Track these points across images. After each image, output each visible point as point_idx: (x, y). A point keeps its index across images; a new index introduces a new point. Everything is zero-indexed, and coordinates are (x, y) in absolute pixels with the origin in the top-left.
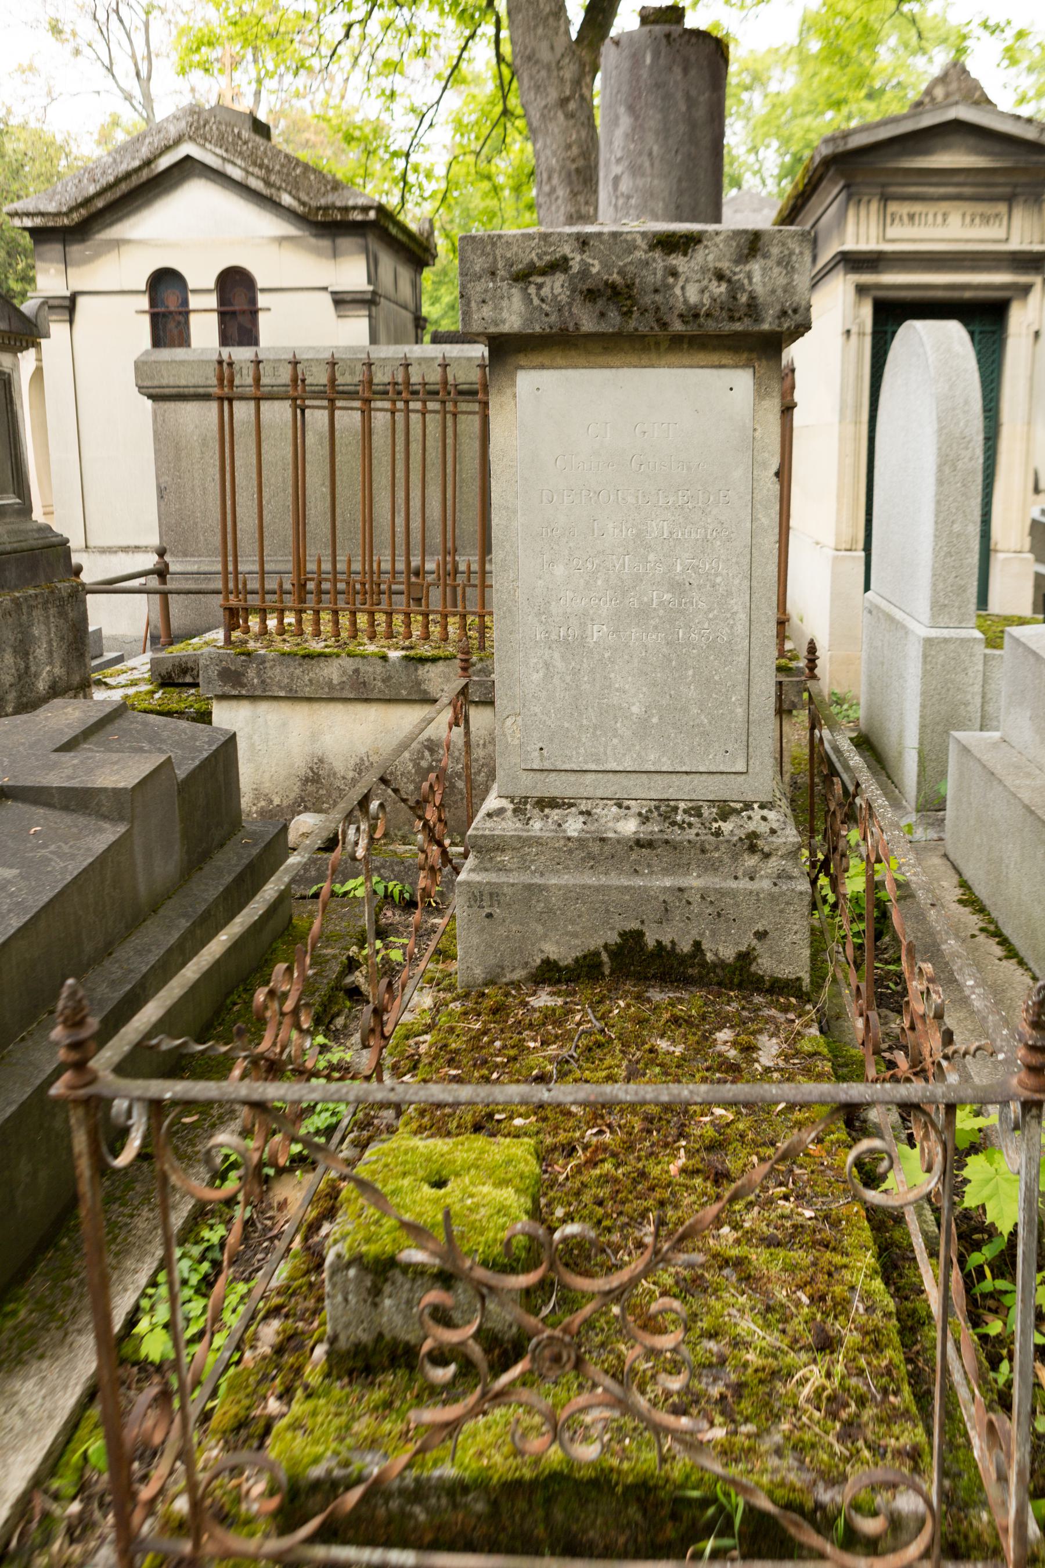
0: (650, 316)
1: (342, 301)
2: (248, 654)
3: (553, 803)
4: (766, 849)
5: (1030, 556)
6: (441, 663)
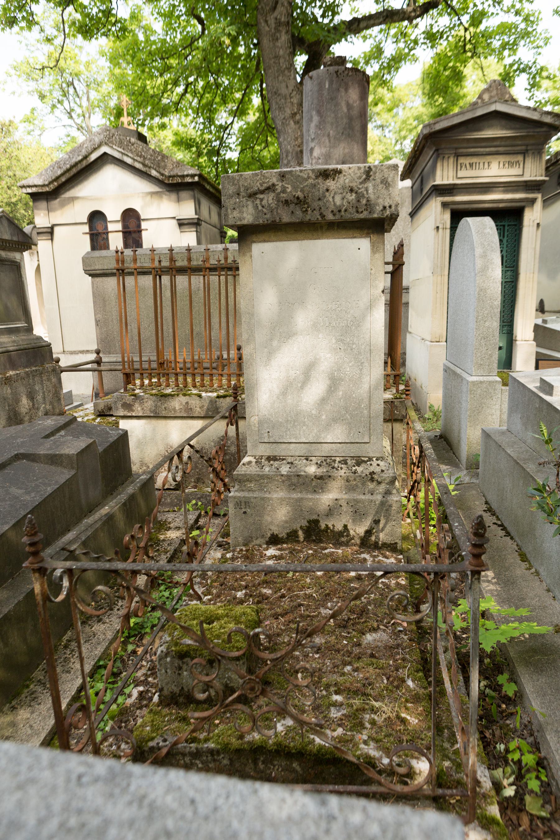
0: (317, 213)
1: (182, 224)
2: (135, 395)
3: (275, 458)
4: (379, 480)
5: (534, 343)
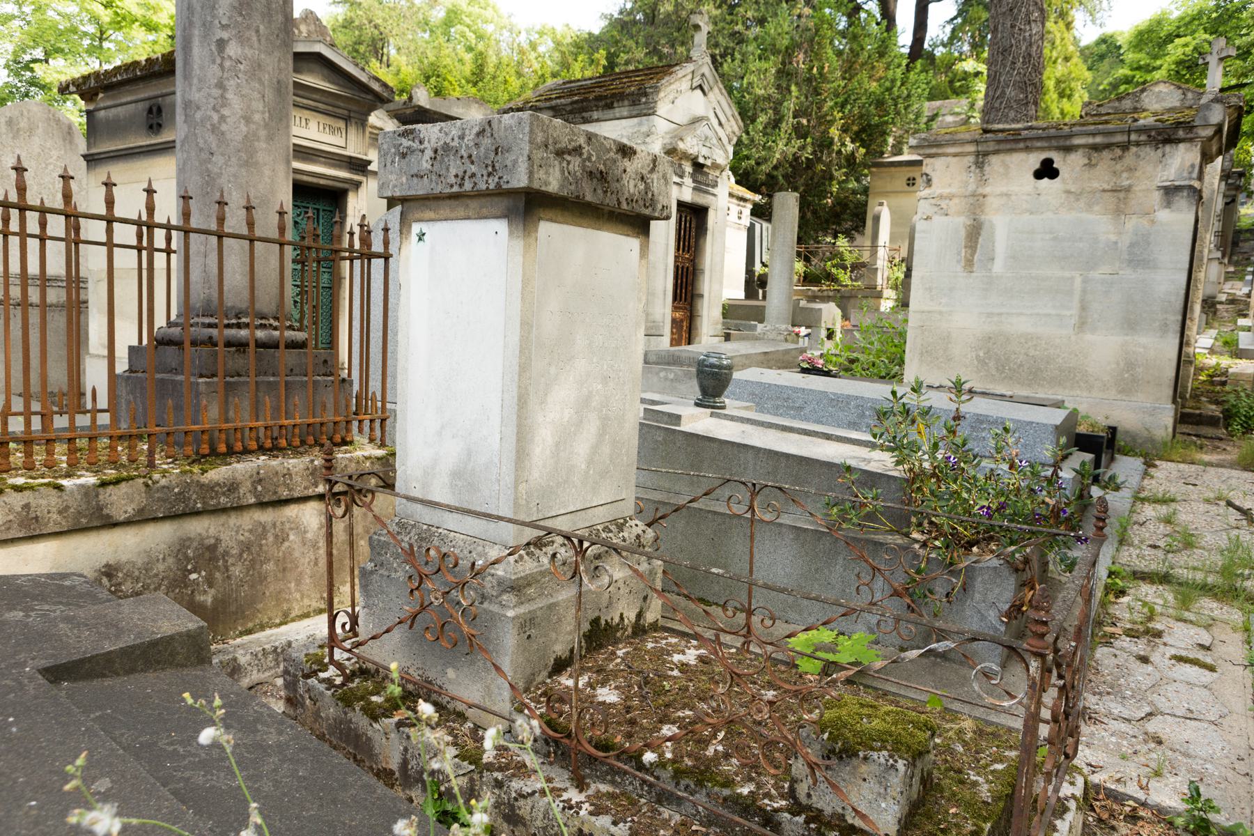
6: (123, 484)
